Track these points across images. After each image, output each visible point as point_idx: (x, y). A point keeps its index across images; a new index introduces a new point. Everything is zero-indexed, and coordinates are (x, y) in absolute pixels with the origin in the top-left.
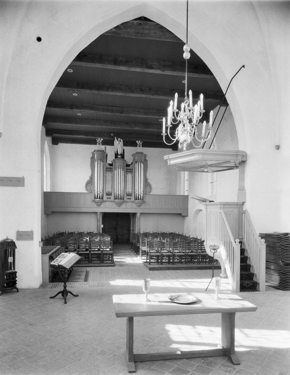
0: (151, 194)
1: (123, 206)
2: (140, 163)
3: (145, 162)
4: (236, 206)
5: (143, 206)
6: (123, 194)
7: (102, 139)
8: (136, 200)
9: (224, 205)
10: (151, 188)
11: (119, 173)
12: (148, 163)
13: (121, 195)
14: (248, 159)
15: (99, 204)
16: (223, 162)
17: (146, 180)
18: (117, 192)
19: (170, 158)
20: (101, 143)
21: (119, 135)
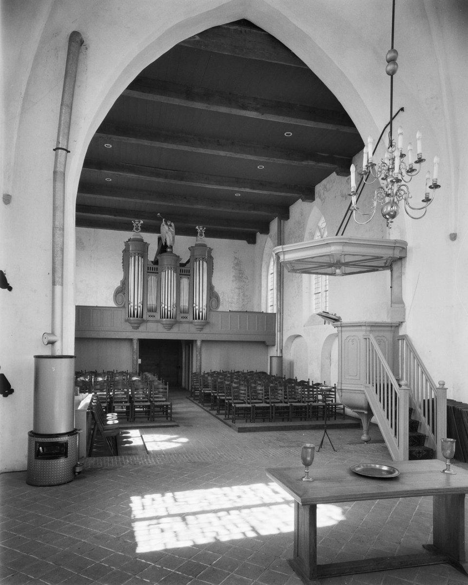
0: (218, 310)
1: (175, 329)
2: (201, 262)
3: (210, 261)
4: (389, 329)
5: (207, 330)
6: (175, 310)
7: (142, 222)
8: (196, 319)
9: (372, 326)
10: (218, 301)
11: (169, 277)
12: (214, 261)
13: (172, 311)
14: (408, 254)
15: (136, 325)
16: (371, 257)
17: (211, 288)
18: (166, 307)
19: (285, 250)
20: (140, 228)
21: (170, 216)
